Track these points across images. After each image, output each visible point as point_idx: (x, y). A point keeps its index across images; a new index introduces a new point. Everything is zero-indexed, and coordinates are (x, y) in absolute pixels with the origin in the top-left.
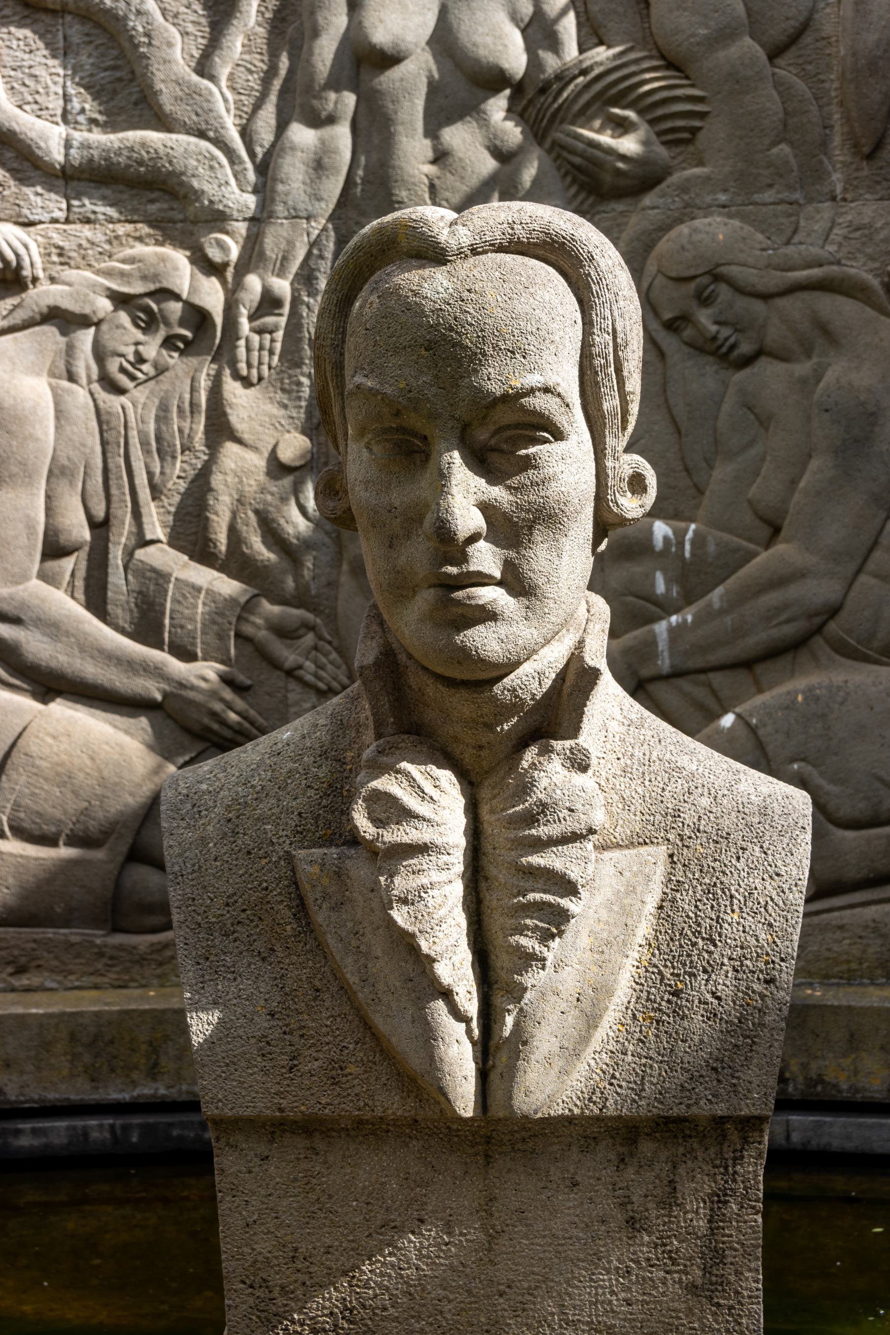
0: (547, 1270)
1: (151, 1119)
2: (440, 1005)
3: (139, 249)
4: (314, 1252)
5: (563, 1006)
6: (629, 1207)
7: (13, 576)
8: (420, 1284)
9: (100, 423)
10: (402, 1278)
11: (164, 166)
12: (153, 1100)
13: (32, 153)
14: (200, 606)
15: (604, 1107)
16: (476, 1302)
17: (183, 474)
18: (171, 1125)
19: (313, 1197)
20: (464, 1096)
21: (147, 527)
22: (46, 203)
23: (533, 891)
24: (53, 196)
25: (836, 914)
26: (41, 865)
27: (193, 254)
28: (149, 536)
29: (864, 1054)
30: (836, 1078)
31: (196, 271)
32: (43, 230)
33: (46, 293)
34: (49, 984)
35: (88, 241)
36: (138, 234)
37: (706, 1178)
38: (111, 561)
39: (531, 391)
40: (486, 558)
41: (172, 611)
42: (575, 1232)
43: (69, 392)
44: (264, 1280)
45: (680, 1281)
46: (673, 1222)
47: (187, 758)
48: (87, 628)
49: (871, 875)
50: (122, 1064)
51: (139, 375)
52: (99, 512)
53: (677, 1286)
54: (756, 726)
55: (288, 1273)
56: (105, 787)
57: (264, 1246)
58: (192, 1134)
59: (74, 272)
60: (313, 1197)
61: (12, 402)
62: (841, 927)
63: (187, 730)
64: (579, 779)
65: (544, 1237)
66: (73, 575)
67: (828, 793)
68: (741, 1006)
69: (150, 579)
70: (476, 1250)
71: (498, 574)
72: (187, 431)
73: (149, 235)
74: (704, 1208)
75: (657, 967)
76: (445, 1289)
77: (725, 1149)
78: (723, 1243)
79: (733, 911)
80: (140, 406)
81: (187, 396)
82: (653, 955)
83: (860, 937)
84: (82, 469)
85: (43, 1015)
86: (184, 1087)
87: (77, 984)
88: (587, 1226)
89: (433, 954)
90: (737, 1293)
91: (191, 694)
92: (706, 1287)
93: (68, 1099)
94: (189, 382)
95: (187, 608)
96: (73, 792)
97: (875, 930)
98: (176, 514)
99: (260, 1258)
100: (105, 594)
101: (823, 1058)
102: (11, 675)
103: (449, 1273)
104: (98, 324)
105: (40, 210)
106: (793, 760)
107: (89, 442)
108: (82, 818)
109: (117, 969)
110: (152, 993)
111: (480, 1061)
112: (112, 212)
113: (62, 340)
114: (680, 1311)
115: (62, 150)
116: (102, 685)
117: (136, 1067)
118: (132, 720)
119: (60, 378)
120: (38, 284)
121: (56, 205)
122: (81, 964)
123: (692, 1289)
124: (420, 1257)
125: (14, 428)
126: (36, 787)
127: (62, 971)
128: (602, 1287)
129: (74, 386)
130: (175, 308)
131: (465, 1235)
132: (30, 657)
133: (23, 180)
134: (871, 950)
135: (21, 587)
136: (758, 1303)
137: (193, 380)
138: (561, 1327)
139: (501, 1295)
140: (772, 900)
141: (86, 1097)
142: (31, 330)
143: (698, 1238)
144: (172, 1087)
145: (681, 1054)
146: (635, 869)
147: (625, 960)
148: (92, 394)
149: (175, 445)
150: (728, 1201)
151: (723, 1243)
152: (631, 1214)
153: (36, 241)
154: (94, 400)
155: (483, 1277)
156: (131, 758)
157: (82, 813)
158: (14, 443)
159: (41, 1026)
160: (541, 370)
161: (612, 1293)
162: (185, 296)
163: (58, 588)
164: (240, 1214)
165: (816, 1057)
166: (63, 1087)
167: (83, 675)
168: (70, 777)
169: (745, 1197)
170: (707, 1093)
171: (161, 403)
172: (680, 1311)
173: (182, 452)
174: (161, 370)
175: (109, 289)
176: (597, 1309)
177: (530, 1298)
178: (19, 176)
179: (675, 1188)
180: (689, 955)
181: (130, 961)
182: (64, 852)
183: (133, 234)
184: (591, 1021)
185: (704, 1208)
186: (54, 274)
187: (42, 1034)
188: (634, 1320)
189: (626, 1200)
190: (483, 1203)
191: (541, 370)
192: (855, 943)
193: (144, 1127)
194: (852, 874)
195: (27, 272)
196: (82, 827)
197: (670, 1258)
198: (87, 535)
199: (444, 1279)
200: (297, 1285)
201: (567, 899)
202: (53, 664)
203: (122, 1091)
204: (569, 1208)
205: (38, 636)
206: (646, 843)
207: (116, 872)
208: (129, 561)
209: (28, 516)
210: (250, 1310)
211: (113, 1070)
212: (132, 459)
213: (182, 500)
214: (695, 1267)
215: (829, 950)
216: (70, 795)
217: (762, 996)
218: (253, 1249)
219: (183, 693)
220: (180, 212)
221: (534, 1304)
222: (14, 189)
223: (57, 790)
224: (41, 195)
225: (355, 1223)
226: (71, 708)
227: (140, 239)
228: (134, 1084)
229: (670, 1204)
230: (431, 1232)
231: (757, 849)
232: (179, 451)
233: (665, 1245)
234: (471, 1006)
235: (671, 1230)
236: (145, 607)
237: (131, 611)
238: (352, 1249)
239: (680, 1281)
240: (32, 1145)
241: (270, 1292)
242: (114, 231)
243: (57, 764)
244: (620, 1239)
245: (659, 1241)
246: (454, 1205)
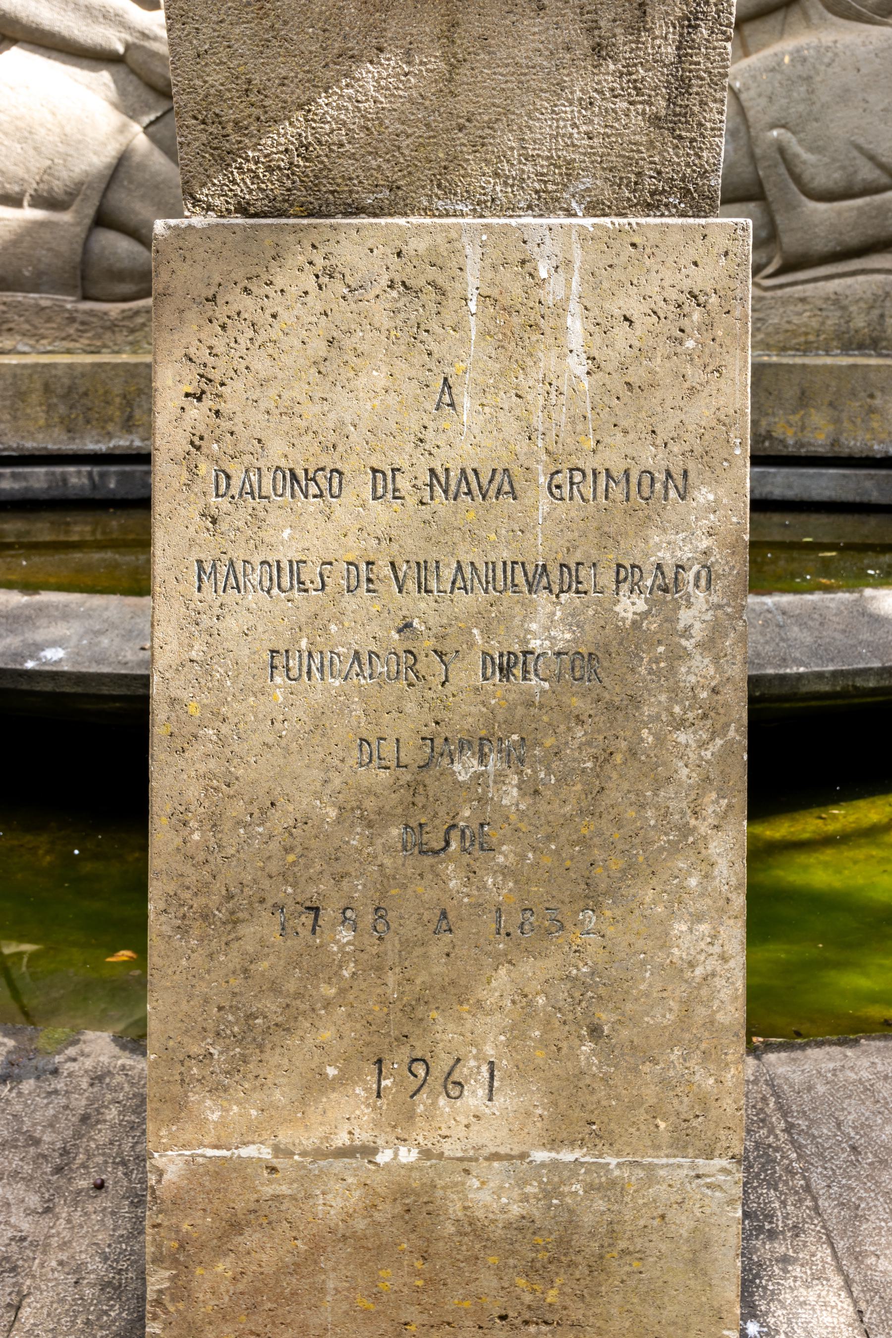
0: (509, 101)
1: (128, 468)
4: (268, 84)
6: (596, 32)
8: (378, 118)
10: (360, 111)
12: (129, 452)
16: (434, 137)
19: (267, 23)
25: (800, 288)
26: (6, 226)
29: (812, 410)
30: (784, 433)
34: (21, 348)
42: (539, 60)
44: (217, 115)
45: (644, 113)
46: (640, 49)
47: (152, 117)
49: (838, 248)
50: (97, 416)
53: (640, 118)
54: (739, 90)
55: (242, 106)
56: (68, 145)
57: (216, 78)
60: (267, 23)
62: (803, 300)
65: (507, 65)
67: (804, 163)
70: (436, 81)
74: (674, 33)
76: (403, 124)
83: (821, 310)
85: (16, 365)
87: (49, 348)
88: (552, 53)
90: (700, 124)
92: (669, 118)
93: (46, 448)
96: (35, 149)
97: (836, 302)
99: (212, 91)
101: (774, 415)
103: (408, 105)
106: (773, 126)
108: (46, 177)
109: (89, 335)
114: (641, 144)
117: (111, 419)
122: (53, 328)
123: (655, 120)
127: (34, 335)
128: (564, 120)
131: (425, 64)
134: (829, 322)
136: (721, 136)
138: (520, 162)
139: (460, 130)
141: (64, 447)
150: (699, 26)
152: (598, 40)
155: (442, 109)
159: (15, 376)
161: (574, 125)
164: (191, 43)
165: (767, 414)
166: (40, 436)
167: (38, 20)
168: (30, 133)
169: (716, 21)
172: (641, 144)
177: (490, 131)
179: (645, 13)
181: (102, 327)
182: (30, 214)
185: (674, 33)
187: (18, 387)
188: (594, 154)
189: (594, 25)
190: (444, 28)
192: (815, 315)
194: (821, 246)
196: (46, 187)
197: (635, 88)
200: (251, 120)
203: (98, 442)
204: (534, 34)
207: (83, 236)
210: (202, 147)
211: (88, 422)
214: (659, 98)
215: (789, 322)
216: (31, 152)
218: (205, 82)
219: (147, 44)
221: (494, 137)
223: (18, 146)
225: (311, 52)
228: (110, 435)
229: (639, 30)
230: (391, 61)
233: (630, 74)
238: (308, 81)
239: (644, 113)
240: (12, 489)
241: (223, 128)
243: (17, 118)
244: (585, 68)
245: (625, 70)
246: (414, 31)
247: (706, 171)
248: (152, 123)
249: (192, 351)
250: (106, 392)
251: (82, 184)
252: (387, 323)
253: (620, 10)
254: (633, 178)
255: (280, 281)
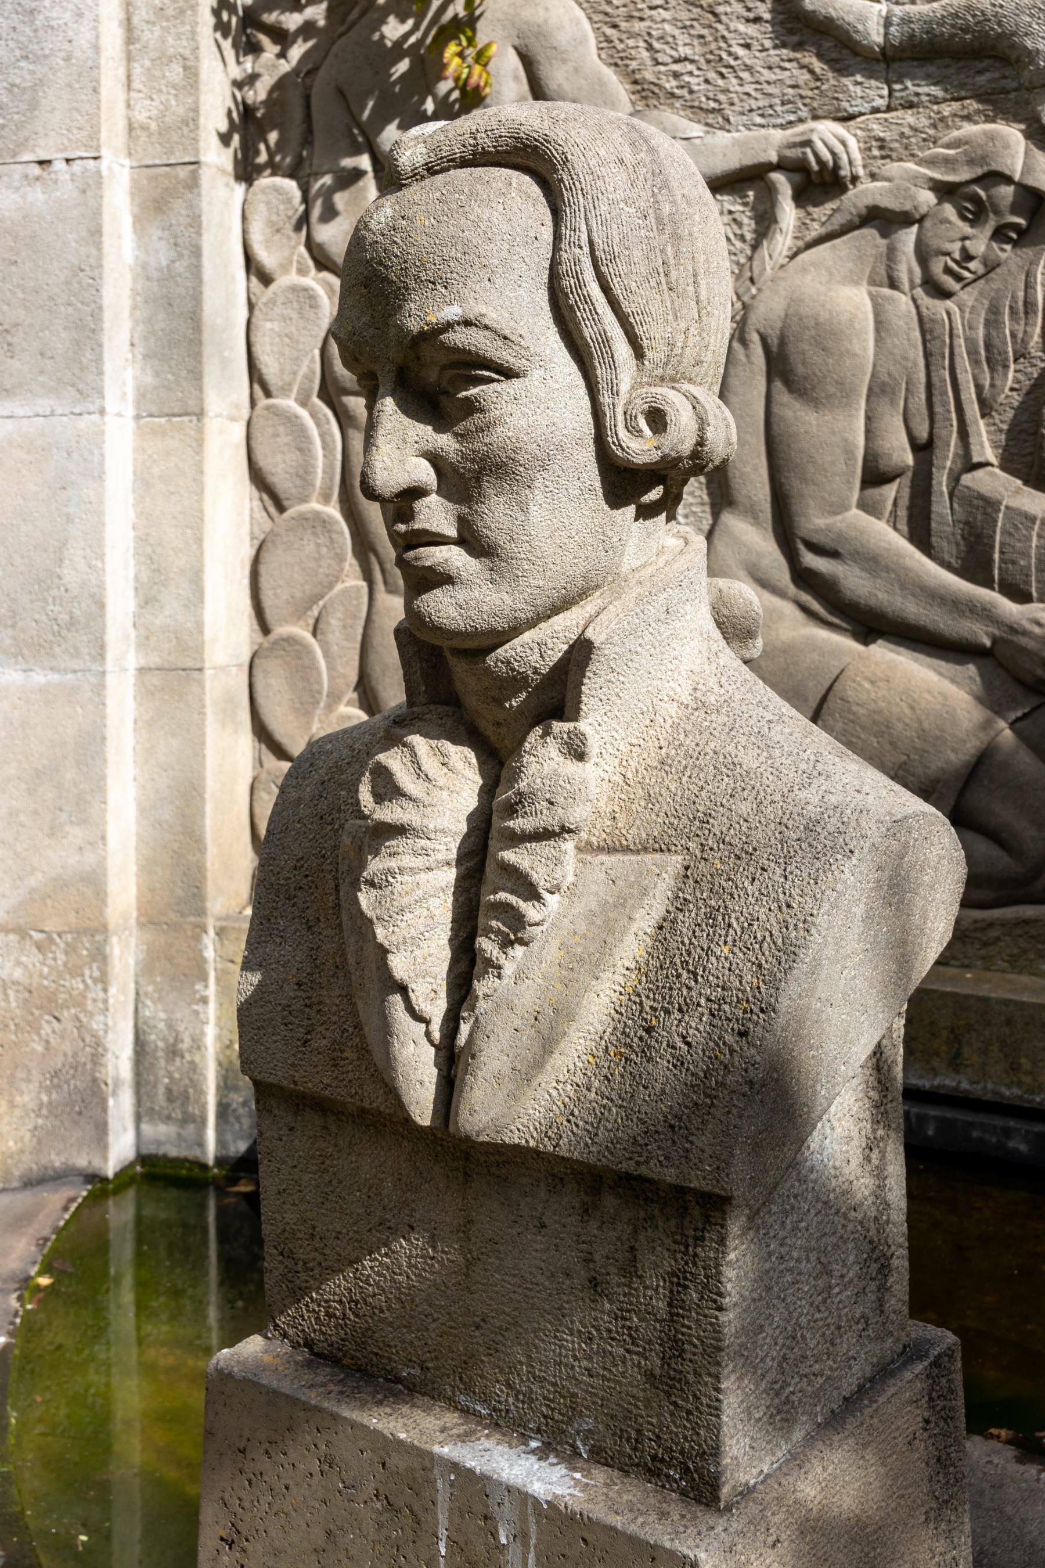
2: (397, 998)
3: (969, 129)
5: (518, 1023)
6: (591, 1265)
7: (831, 506)
9: (923, 332)
11: (992, 29)
13: (850, 38)
14: (1035, 538)
15: (558, 1145)
17: (1016, 386)
18: (972, 1124)
20: (421, 1100)
21: (974, 448)
22: (864, 91)
23: (503, 890)
24: (874, 83)
27: (1029, 126)
28: (976, 459)
31: (1032, 147)
32: (863, 122)
33: (865, 192)
35: (911, 127)
36: (965, 112)
37: (666, 1254)
38: (935, 488)
39: (449, 326)
40: (436, 514)
41: (1002, 544)
42: (541, 1279)
43: (891, 300)
47: (1019, 714)
48: (908, 562)
50: (921, 1047)
51: (966, 274)
52: (922, 432)
53: (636, 1370)
58: (994, 1140)
59: (896, 164)
61: (827, 316)
63: (1020, 682)
64: (572, 767)
65: (515, 1276)
66: (895, 503)
68: (710, 1058)
69: (977, 508)
71: (452, 532)
72: (1020, 335)
73: (978, 112)
74: (664, 1288)
75: (639, 996)
77: (686, 1224)
78: (683, 1334)
79: (726, 943)
80: (968, 310)
81: (1021, 294)
82: (640, 982)
84: (904, 385)
86: (990, 1086)
89: (386, 944)
91: (1023, 641)
94: (1023, 277)
95: (1019, 541)
96: (891, 743)
98: (1009, 431)
100: (929, 524)
102: (831, 613)
103: (433, 1290)
104: (920, 221)
105: (859, 101)
107: (911, 355)
110: (969, 976)
111: (445, 1069)
112: (936, 91)
113: (883, 242)
115: (882, 30)
116: (925, 627)
117: (937, 1054)
118: (958, 667)
119: (880, 286)
120: (858, 184)
121: (877, 92)
124: (410, 1266)
125: (830, 344)
126: (853, 736)
129: (895, 293)
130: (1006, 193)
132: (848, 593)
133: (841, 69)
135: (839, 518)
137: (1028, 275)
138: (528, 1379)
140: (771, 935)
142: (850, 235)
143: (656, 1320)
144: (977, 1083)
145: (640, 1102)
146: (632, 879)
147: (594, 983)
148: (914, 300)
149: (1007, 353)
151: (683, 1334)
152: (593, 1273)
153: (855, 135)
154: (917, 307)
156: (954, 710)
157: (900, 767)
158: (830, 361)
160: (462, 301)
162: (1017, 177)
163: (879, 519)
167: (905, 615)
168: (888, 727)
169: (706, 1286)
170: (660, 1152)
171: (991, 304)
173: (1016, 360)
174: (991, 266)
175: (931, 179)
176: (560, 1371)
177: (501, 1339)
178: (837, 66)
180: (671, 989)
183: (960, 113)
184: (548, 1045)
186: (875, 170)
189: (589, 1257)
191: (462, 301)
193: (941, 1121)
195: (845, 172)
197: (630, 1335)
198: (909, 459)
199: (429, 1295)
201: (530, 903)
202: (873, 602)
203: (921, 1077)
204: (536, 1251)
205: (857, 571)
206: (662, 851)
208: (954, 488)
209: (846, 440)
212: (958, 371)
213: (1015, 416)
216: (887, 746)
217: (732, 1051)
219: (1014, 638)
220: (1013, 80)
222: (832, 82)
224: (861, 83)
226: (892, 651)
227: (968, 118)
228: (935, 1073)
231: (779, 871)
232: (1012, 359)
234: (436, 1009)
235: (631, 1303)
236: (972, 539)
237: (958, 544)
242: (939, 113)
247: (704, 1453)
248: (1018, 720)
249: (227, 1496)
250: (932, 1023)
251: (938, 782)
252: (372, 1534)
253: (613, 1248)
254: (633, 1435)
255: (293, 1456)
